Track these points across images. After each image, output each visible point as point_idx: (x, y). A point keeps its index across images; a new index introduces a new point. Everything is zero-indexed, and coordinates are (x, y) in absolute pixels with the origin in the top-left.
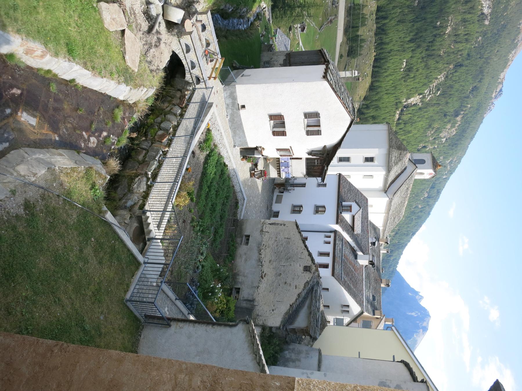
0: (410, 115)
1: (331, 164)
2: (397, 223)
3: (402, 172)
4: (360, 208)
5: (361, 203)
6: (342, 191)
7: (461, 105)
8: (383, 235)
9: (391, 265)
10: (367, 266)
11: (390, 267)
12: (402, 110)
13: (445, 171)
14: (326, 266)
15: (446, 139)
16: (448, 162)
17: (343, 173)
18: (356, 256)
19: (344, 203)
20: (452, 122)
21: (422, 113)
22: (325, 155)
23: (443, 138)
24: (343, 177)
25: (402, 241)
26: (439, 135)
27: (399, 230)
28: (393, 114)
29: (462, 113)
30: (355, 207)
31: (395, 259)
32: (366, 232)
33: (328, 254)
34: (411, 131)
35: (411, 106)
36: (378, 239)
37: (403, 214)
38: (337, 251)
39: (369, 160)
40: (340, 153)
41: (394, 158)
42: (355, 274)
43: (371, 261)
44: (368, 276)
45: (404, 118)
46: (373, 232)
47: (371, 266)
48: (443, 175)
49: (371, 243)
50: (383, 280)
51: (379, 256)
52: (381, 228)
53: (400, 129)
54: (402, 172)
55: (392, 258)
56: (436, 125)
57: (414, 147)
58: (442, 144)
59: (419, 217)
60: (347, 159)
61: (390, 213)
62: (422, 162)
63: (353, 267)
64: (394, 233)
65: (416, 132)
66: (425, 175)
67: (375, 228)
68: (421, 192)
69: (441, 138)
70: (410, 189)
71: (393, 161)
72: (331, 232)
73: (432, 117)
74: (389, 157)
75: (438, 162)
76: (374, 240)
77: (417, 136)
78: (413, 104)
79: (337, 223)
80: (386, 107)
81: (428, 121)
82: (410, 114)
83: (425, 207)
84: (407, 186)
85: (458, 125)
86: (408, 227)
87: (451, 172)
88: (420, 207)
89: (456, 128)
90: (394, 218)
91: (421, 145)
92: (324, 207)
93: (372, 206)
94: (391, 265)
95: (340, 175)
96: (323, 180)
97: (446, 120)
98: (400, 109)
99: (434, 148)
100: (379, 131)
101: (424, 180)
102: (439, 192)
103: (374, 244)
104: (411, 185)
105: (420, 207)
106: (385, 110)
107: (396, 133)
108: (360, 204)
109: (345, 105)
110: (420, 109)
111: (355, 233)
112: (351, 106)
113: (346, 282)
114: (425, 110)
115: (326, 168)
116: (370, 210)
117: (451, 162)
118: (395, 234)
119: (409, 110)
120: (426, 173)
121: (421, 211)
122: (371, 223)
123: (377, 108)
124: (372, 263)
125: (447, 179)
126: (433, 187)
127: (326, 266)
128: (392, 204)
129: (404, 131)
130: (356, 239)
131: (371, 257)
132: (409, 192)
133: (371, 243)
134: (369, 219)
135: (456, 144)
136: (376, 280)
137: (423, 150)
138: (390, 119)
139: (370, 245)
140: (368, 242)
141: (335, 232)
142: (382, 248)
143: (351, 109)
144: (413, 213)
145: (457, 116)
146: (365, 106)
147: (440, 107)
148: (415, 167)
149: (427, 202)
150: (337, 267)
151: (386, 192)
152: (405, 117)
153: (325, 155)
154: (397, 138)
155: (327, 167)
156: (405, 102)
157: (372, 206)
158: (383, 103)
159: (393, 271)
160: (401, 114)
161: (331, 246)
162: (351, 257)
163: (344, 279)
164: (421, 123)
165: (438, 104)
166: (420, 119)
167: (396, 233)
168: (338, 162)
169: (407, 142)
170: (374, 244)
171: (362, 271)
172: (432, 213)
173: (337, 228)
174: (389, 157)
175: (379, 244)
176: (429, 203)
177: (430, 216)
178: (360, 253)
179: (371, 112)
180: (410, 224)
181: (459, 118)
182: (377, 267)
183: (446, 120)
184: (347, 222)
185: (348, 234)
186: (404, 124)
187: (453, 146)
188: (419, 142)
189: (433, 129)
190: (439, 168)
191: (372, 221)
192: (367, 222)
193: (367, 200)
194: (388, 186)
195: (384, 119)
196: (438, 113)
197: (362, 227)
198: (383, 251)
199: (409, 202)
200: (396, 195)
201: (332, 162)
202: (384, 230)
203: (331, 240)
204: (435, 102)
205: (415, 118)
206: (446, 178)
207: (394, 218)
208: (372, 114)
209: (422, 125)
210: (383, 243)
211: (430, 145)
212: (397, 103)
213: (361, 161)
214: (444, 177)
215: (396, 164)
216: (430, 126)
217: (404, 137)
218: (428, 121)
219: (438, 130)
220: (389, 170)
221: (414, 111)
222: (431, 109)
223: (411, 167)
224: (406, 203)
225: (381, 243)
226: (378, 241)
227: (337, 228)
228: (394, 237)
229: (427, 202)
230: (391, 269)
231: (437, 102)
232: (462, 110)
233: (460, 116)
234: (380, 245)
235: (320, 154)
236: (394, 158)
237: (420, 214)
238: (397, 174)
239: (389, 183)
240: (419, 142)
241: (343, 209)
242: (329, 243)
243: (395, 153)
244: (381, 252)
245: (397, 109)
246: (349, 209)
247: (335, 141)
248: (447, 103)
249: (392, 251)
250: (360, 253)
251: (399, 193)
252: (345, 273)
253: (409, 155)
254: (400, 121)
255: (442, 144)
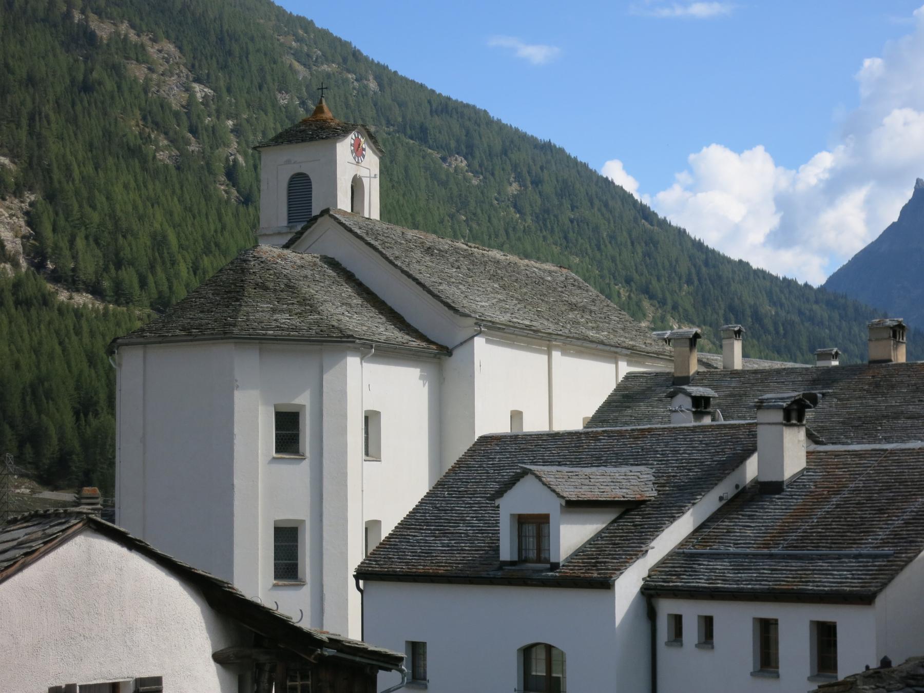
0: (80, 243)
1: (306, 625)
2: (594, 292)
3: (349, 277)
4: (525, 472)
5: (499, 468)
6: (444, 562)
7: (43, 20)
8: (658, 356)
9: (800, 313)
10: (809, 435)
11: (811, 319)
12: (56, 277)
13: (345, 81)
14: (825, 635)
15: (198, 80)
16: (302, 71)
17: (356, 556)
18: (768, 489)
19: (506, 552)
20: (117, 59)
21: (69, 187)
22: (263, 658)
23: (192, 95)
24: (371, 557)
25: (684, 267)
26: (176, 115)
27: (628, 281)
28: (70, 321)
29: (77, 16)
30: (524, 499)
31: (770, 294)
32: (647, 443)
33: (766, 632)
34: (154, 236)
35: (38, 236)
36: (677, 383)
37: (548, 266)
38: (747, 580)
39: (288, 432)
40: (255, 581)
41: (283, 318)
42: (857, 490)
43: (787, 418)
44: (863, 426)
45: (91, 269)
46: (643, 408)
47: (809, 414)
48: (363, 92)
49: (698, 414)
50: (876, 351)
51: (762, 377)
52: (625, 368)
53: (143, 283)
54: (349, 277)
55: (767, 309)
56: (132, 126)
57: (229, 219)
58: (218, 98)
59: (565, 190)
60: (286, 539)
61: (552, 328)
62: (300, 187)
63: (820, 500)
64: (646, 304)
65: (159, 215)
66: (362, 172)
67: (624, 397)
68: (444, 184)
69: (190, 105)
70: (431, 239)
71: (296, 321)
72: (652, 615)
73: (91, 146)
74: (275, 339)
75: (302, 114)
76: (685, 402)
77: (177, 209)
78: (26, 230)
79: (606, 585)
80: (36, 351)
81: (111, 161)
82: (72, 242)
83: (515, 167)
84: (418, 254)
85: (133, 36)
86: (612, 237)
87: (351, 57)
88: (514, 189)
89: (145, 39)
90: (573, 307)
91: (221, 188)
92: (527, 652)
93: (516, 416)
94: (800, 313)
95: (361, 574)
96: (391, 662)
97: (110, 85)
98: (50, 287)
99: (236, 131)
100: (150, 389)
101: (385, 171)
102: (446, 108)
103: (701, 405)
104: (411, 234)
105: (514, 189)
106: (51, 357)
107: (161, 304)
108: (507, 474)
109: (14, 560)
110: (50, 197)
111: (651, 493)
112: (20, 534)
113: (896, 535)
114: (57, 175)
115: (329, 652)
116: (534, 424)
117: (305, 59)
118: (652, 297)
119: (56, 247)
120: (354, 171)
121: (536, 183)
122: (601, 416)
123: (38, 392)
124: (794, 414)
125: (383, 74)
126: (422, 134)
127: (825, 635)
128: (503, 318)
129: (152, 267)
130: (680, 488)
131: (764, 416)
132: (445, 243)
133: (698, 414)
134: (578, 426)
135: (221, 40)
136: (877, 387)
137: (246, 178)
138: (92, 334)
139: (707, 421)
140: (693, 430)
141: (650, 593)
142: (717, 360)
143: (36, 531)
144: (544, 217)
145: (91, 38)
146: (28, 449)
147: (48, 109)
148: (325, 221)
149: (490, 155)
150: (827, 583)
151: (446, 351)
152: (89, 263)
153: (263, 658)
154: (184, 305)
155: (320, 643)
156: (16, 265)
157: (516, 416)
158: (17, 366)
159: (831, 304)
160: (73, 283)
161: (718, 610)
162: (773, 511)
163: (885, 543)
164: (118, 191)
165: (32, 118)
166: (101, 199)
167: (646, 291)
168: (302, 584)
169: (207, 251)
170: (701, 405)
171: (837, 455)
172: (542, 135)
173: (628, 584)
174: (275, 339)
175: (699, 379)
176: (498, 147)
177: (558, 142)
178: (752, 469)
179: (60, 419)
180: (596, 229)
181: (103, 30)
182: (815, 382)
183: (110, 85)
184: (599, 536)
185: (657, 529)
186: (119, 265)
187: (230, 53)
188: (208, 198)
189: (147, 140)
190: (328, 114)
191: (591, 412)
192: (595, 437)
193: (484, 440)
194: (415, 343)
195: (92, 360)
196: (74, 120)
197: (620, 460)
198: (737, 357)
199: (491, 240)
200: (462, 303)
201: (295, 620)
202: (633, 354)
203: (691, 612)
204: (23, 135)
205: (95, 217)
206: (378, 78)
207: (573, 307)
208: (69, 419)
209: (126, 186)
210: (695, 356)
211: (222, 152)
212: (18, 303)
213: (296, 473)
214: (373, 85)
215: (308, 305)
216: (133, 152)
217: (183, 269)
218: (111, 161)
219: (155, 116)
220: (340, 341)
221: (62, 222)
222: (54, 147)
223: (328, 241)
224: (497, 254)
225: (694, 368)
226: (686, 380)
227: (628, 584)
228: (663, 303)
229: (490, 155)
230: (820, 311)
231: (24, 122)
232: (68, 16)
233: (93, 23)
234: (710, 375)
235: (257, 681)
236: (283, 318)
237: (548, 188)
238: (357, 301)
239: (399, 336)
240: (208, 198)
241: (532, 554)
242: (708, 623)
243: (259, 311)
244: (738, 363)
245: (46, 301)
246: (534, 527)
247: (188, 609)
248: (31, 81)
249: (734, 311)
250: (752, 469)
251: (450, 291)
252: (854, 542)
253: (268, 250)
254: (106, 284)
255: (218, 98)
